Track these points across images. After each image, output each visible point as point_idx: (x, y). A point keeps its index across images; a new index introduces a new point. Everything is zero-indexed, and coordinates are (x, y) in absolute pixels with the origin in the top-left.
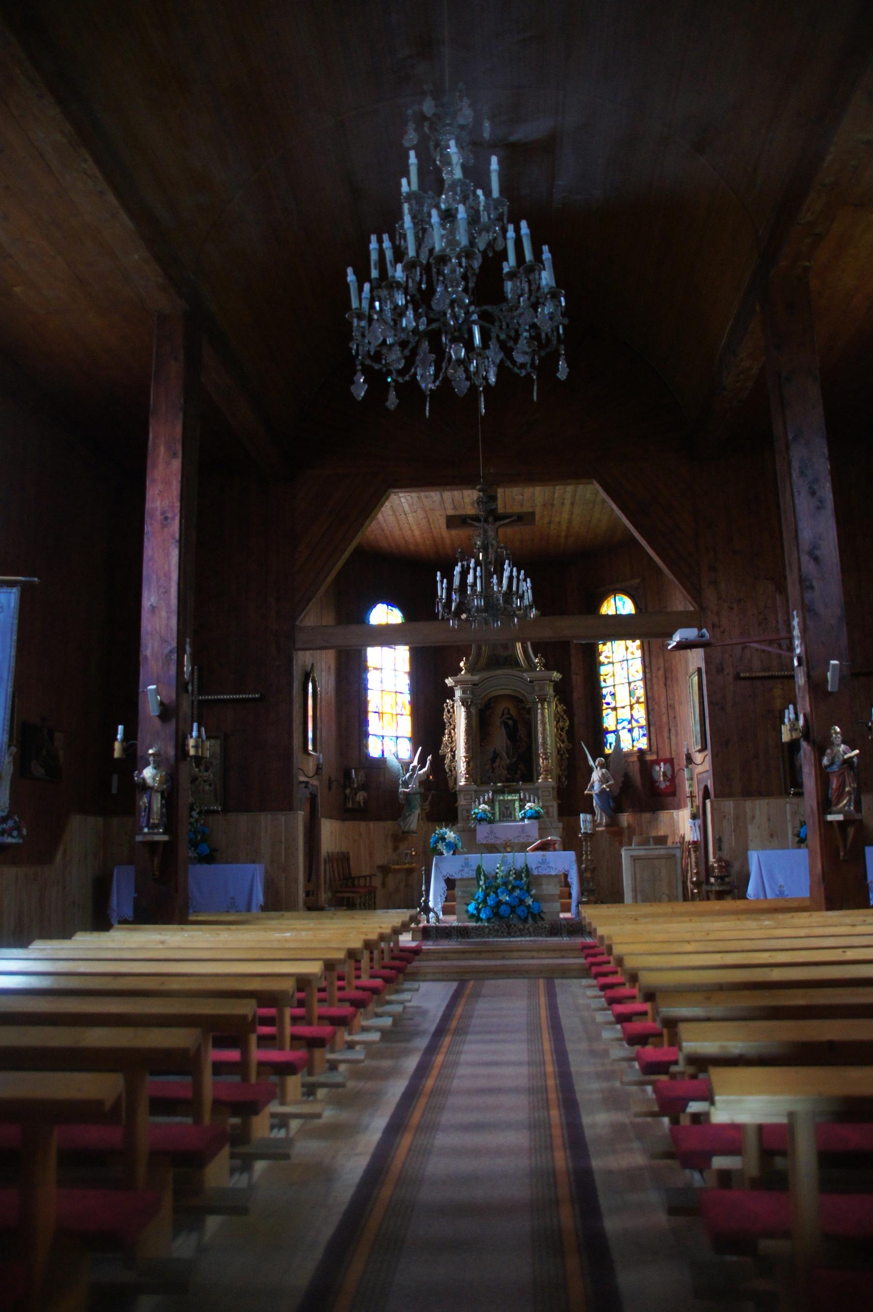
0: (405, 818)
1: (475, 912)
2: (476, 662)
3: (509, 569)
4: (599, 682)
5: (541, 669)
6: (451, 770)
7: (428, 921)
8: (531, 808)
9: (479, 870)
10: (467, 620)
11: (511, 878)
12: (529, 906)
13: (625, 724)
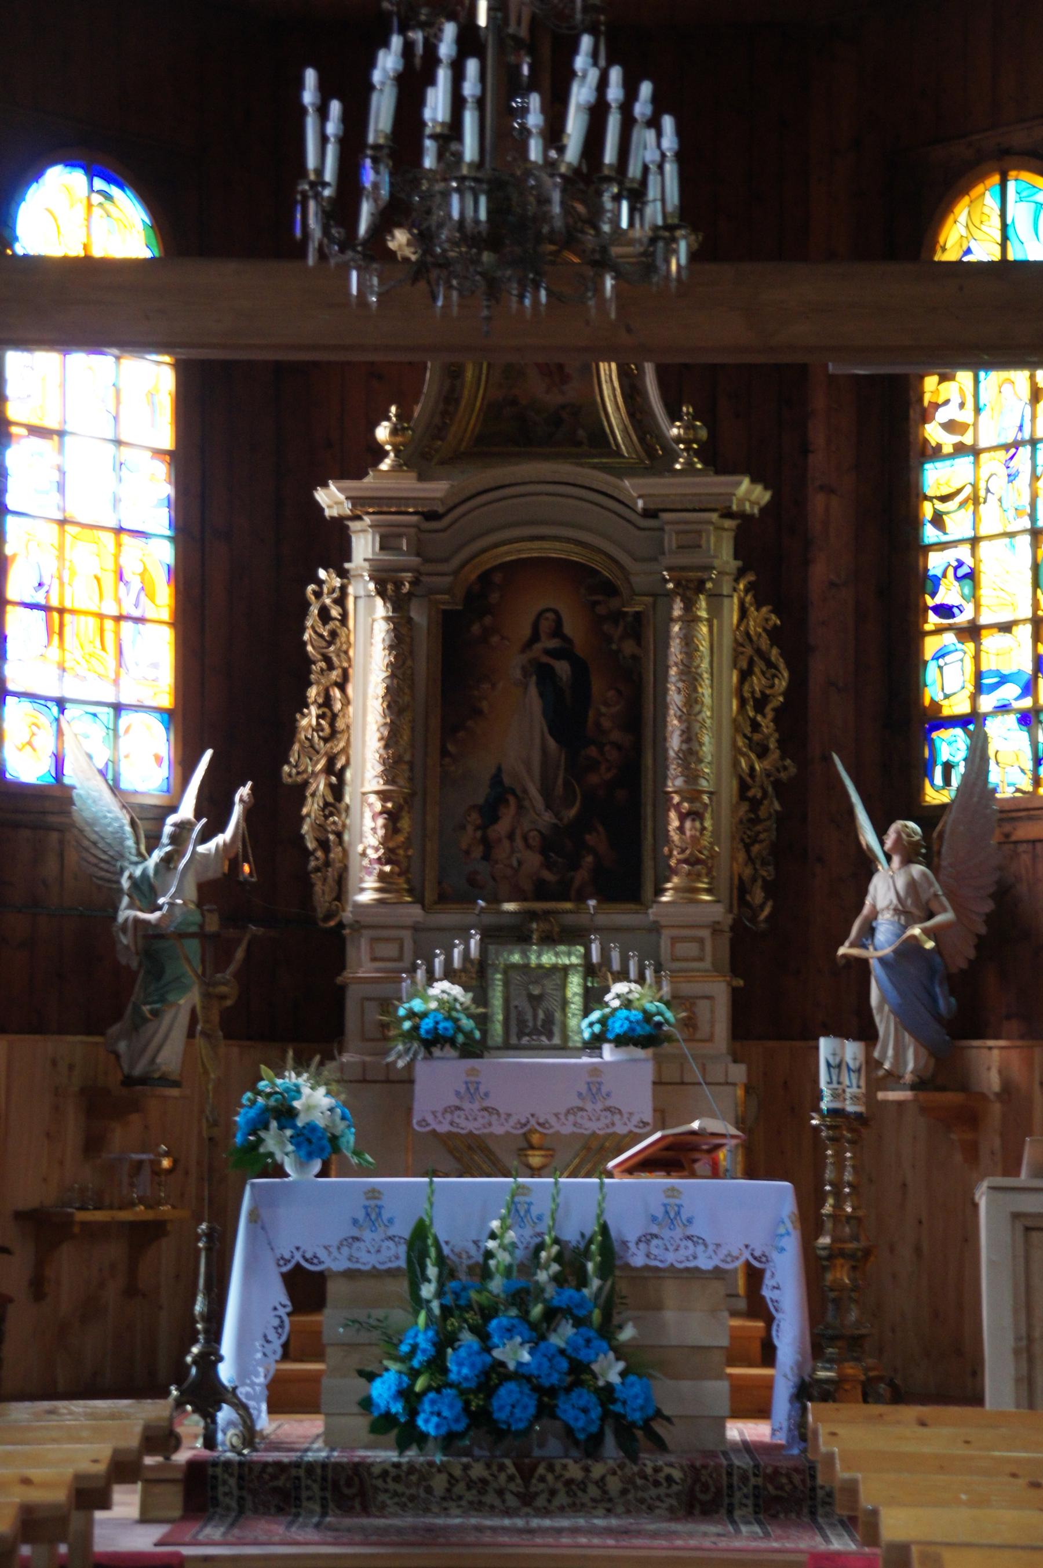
0: (139, 1022)
1: (397, 1408)
2: (437, 431)
3: (593, 75)
4: (915, 524)
5: (689, 470)
6: (324, 845)
7: (210, 1442)
8: (627, 1004)
9: (419, 1239)
10: (419, 271)
11: (542, 1276)
12: (609, 1387)
13: (1010, 692)
